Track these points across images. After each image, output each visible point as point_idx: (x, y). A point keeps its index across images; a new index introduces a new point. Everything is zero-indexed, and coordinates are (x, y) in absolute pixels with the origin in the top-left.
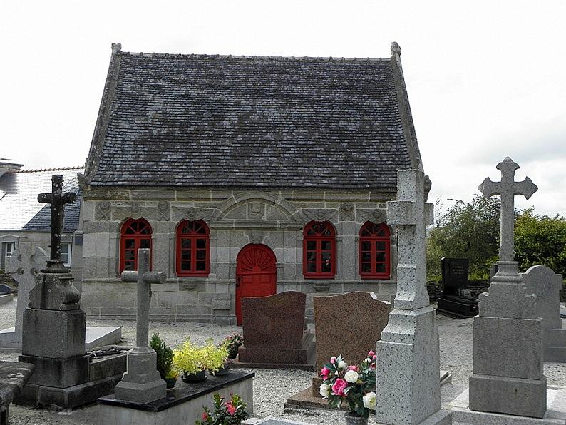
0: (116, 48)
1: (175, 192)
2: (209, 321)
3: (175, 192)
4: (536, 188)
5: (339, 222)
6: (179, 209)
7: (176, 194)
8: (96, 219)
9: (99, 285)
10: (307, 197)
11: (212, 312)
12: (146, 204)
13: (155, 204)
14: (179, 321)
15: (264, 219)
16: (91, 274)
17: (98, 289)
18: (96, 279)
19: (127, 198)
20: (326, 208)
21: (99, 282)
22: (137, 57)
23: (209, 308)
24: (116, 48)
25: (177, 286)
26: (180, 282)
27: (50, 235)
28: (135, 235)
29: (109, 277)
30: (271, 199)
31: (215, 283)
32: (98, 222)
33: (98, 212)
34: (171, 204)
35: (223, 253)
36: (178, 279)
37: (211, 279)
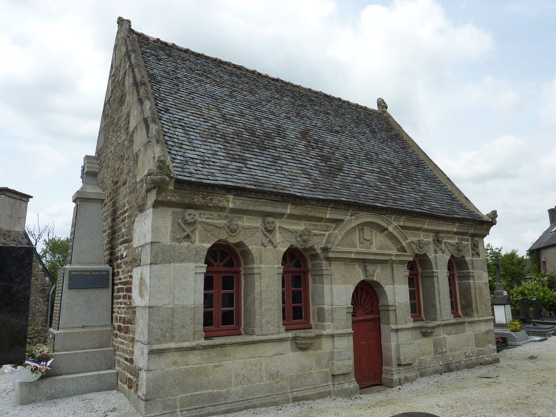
0: (126, 31)
1: (289, 206)
2: (329, 393)
3: (289, 206)
4: (26, 198)
5: (433, 255)
6: (287, 233)
7: (289, 209)
8: (174, 239)
9: (176, 357)
10: (418, 226)
11: (330, 378)
12: (245, 222)
13: (257, 223)
14: (296, 399)
15: (374, 249)
16: (163, 336)
17: (174, 364)
18: (172, 345)
19: (223, 209)
20: (470, 243)
21: (178, 350)
22: (155, 41)
23: (326, 374)
24: (126, 31)
25: (287, 345)
26: (294, 338)
27: (351, 339)
28: (225, 267)
29: (194, 339)
30: (384, 224)
31: (332, 336)
32: (177, 244)
33: (177, 226)
34: (278, 223)
35: (335, 293)
36: (290, 335)
37: (328, 331)
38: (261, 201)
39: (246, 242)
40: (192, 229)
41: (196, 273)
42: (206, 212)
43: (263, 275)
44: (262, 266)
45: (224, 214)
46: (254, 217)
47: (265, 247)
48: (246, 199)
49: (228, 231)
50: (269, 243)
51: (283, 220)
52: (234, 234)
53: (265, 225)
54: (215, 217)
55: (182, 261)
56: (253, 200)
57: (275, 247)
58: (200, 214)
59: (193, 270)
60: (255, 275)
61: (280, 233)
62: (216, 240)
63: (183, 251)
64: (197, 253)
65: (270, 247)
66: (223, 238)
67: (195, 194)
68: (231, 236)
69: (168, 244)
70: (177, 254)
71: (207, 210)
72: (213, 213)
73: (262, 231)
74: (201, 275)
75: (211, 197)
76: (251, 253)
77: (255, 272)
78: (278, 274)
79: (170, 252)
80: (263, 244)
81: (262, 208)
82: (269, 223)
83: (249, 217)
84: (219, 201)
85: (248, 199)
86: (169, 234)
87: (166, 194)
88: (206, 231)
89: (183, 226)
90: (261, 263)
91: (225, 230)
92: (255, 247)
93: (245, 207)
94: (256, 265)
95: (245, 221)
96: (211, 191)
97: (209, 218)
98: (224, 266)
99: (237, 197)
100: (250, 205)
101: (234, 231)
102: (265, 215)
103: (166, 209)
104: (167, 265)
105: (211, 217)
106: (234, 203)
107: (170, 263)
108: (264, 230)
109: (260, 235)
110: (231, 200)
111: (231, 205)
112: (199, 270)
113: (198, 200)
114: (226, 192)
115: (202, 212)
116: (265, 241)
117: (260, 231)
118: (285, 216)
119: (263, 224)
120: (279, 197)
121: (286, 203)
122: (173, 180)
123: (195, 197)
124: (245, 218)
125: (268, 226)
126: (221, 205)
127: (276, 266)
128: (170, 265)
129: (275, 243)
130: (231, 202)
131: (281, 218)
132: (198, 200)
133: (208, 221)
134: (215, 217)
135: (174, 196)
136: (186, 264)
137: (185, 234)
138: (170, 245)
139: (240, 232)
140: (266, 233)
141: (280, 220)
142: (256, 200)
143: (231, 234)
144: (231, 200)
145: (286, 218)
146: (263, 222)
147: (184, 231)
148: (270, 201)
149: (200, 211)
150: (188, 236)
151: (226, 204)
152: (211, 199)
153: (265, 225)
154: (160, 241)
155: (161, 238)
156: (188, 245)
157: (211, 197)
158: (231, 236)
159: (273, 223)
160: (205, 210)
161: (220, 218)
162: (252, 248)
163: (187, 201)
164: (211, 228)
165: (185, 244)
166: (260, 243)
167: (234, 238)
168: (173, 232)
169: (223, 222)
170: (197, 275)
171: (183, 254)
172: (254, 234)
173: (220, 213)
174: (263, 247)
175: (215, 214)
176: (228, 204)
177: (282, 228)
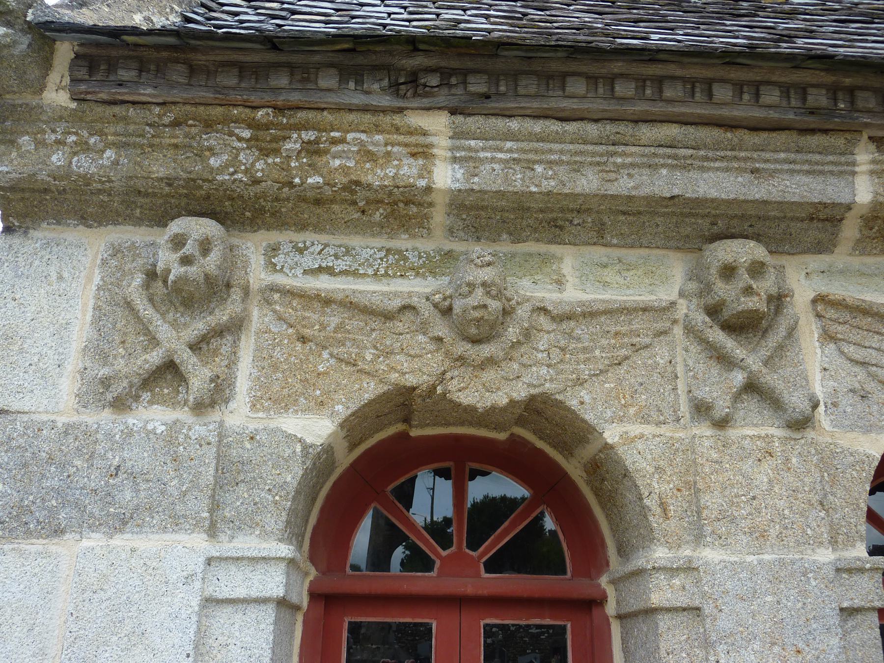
12: (574, 279)
13: (664, 281)
19: (402, 209)
38: (647, 132)
39: (587, 402)
40: (199, 326)
41: (210, 602)
42: (308, 237)
43: (724, 623)
44: (710, 555)
45: (427, 246)
46: (632, 255)
47: (722, 424)
48: (538, 127)
49: (441, 329)
50: (751, 403)
51: (840, 258)
52: (487, 350)
53: (707, 288)
54: (368, 263)
55: (121, 523)
56: (592, 130)
57: (801, 424)
58: (274, 249)
59: (188, 579)
60: (664, 622)
61: (828, 337)
62: (371, 390)
63: (138, 457)
64: (229, 472)
65: (755, 428)
66: (411, 380)
67: (208, 125)
68: (461, 360)
69: (61, 420)
70: (95, 480)
71: (318, 228)
72: (356, 241)
73: (690, 330)
74: (253, 612)
75: (310, 135)
76: (626, 474)
77: (656, 599)
78: (848, 613)
79: (62, 466)
80: (701, 409)
81: (665, 183)
82: (728, 272)
83: (599, 253)
84: (368, 155)
85: (555, 126)
86: (74, 362)
87: (40, 144)
88: (303, 339)
89: (146, 311)
90: (699, 539)
91: (423, 328)
92: (648, 429)
93: (543, 180)
94: (660, 554)
95: (571, 279)
96: (295, 97)
97: (330, 271)
98: (492, 566)
99: (472, 123)
100: (577, 168)
101: (481, 331)
102: (697, 226)
103: (74, 234)
104: (35, 546)
105: (341, 265)
106: (466, 160)
107: (58, 532)
108: (701, 318)
109: (679, 355)
110: (442, 143)
111: (445, 176)
112: (235, 583)
113: (234, 161)
114: (394, 88)
115: (284, 237)
116: (719, 388)
117: (678, 331)
118: (850, 230)
119: (693, 286)
120: (771, 96)
121: (839, 141)
122: (65, 51)
123: (211, 140)
124: (569, 260)
125: (723, 290)
126: (377, 176)
127: (825, 556)
128: (55, 547)
129: (797, 401)
130: (445, 154)
131: (821, 248)
132: (234, 161)
133: (324, 284)
134: (368, 263)
135: (83, 147)
136: (148, 543)
137: (155, 357)
138: (68, 429)
139: (527, 334)
140: (718, 336)
141: (815, 262)
142: (610, 128)
143: (463, 348)
144: (442, 143)
145: (861, 247)
146: (693, 275)
147: (154, 341)
148: (716, 133)
149: (275, 236)
150: (170, 370)
151: (408, 170)
152: (312, 149)
153: (707, 288)
154: (15, 406)
155: (19, 391)
156: (174, 427)
157: (310, 135)
158: (461, 360)
159: (757, 269)
160: (302, 227)
161: (401, 265)
162: (629, 440)
163: (160, 167)
164: (334, 321)
165: (154, 416)
166: (684, 408)
167: (490, 375)
168: (98, 352)
169: (416, 288)
170: (223, 617)
171: (133, 476)
172: (637, 349)
173: (402, 242)
174: (705, 430)
175: (368, 246)
176: (425, 172)
177: (838, 304)
